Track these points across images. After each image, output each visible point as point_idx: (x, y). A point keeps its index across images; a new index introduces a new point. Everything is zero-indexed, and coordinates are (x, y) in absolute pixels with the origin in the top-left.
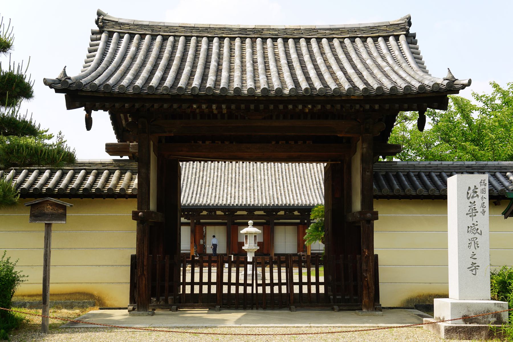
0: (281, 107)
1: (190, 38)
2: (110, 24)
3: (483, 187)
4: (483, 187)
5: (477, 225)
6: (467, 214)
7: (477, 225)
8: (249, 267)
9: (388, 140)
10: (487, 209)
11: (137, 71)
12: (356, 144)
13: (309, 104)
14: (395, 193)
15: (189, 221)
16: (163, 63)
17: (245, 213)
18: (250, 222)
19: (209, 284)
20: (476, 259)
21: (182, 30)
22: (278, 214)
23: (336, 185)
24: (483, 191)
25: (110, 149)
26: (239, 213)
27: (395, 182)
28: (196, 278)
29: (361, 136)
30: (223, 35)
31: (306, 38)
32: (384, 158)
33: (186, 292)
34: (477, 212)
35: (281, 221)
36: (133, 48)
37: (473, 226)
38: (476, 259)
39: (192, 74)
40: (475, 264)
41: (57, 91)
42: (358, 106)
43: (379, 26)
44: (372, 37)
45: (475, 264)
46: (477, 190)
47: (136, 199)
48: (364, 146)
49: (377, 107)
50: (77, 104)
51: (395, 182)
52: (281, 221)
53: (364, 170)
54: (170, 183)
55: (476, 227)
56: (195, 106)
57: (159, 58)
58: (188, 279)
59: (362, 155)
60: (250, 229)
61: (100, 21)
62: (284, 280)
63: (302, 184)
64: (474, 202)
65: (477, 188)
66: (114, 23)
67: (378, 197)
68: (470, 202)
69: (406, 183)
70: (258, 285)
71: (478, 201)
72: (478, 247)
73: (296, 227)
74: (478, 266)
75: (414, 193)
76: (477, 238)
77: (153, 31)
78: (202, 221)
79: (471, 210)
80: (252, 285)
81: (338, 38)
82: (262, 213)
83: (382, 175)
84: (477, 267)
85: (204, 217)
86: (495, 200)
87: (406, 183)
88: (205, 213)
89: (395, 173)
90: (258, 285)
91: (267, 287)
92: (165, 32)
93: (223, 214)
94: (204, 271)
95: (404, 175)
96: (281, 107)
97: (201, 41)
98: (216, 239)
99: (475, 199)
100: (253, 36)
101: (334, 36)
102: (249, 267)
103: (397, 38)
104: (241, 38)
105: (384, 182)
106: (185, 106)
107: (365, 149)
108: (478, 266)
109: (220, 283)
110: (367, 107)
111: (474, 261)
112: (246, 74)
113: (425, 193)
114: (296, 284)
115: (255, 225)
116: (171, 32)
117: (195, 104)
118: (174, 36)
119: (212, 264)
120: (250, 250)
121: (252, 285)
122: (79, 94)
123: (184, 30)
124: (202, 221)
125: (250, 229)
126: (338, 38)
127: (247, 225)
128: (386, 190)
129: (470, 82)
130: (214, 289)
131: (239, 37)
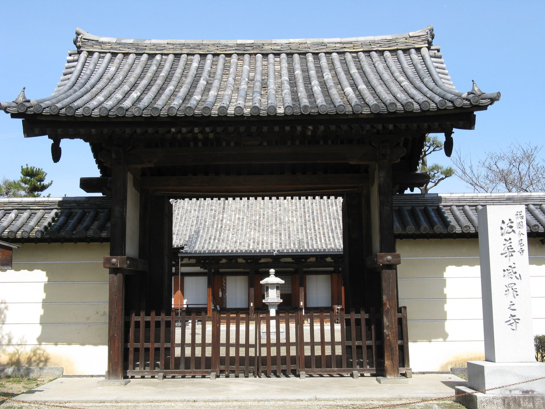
0: (277, 129)
1: (179, 56)
2: (90, 43)
3: (520, 220)
4: (520, 220)
5: (514, 267)
6: (502, 254)
7: (514, 267)
8: (273, 323)
9: (416, 170)
10: (526, 247)
11: (114, 92)
12: (374, 173)
13: (310, 125)
14: (422, 231)
15: (206, 271)
16: (144, 82)
17: (270, 260)
18: (272, 271)
19: (288, 344)
20: (515, 310)
21: (171, 47)
22: (308, 260)
23: (354, 223)
24: (520, 225)
25: (87, 184)
26: (262, 261)
27: (422, 219)
28: (190, 337)
29: (375, 161)
30: (218, 52)
31: (313, 54)
32: (412, 190)
33: (231, 355)
34: (514, 251)
35: (312, 269)
36: (113, 69)
37: (509, 268)
38: (515, 310)
39: (174, 94)
40: (515, 316)
41: (14, 116)
42: (368, 127)
43: (397, 39)
44: (390, 51)
45: (515, 316)
46: (512, 224)
47: (109, 243)
48: (381, 175)
49: (391, 127)
50: (37, 131)
51: (422, 219)
52: (312, 269)
53: (382, 204)
54: (158, 223)
55: (514, 270)
56: (173, 130)
57: (140, 77)
58: (178, 339)
59: (379, 186)
60: (272, 279)
61: (79, 39)
62: (293, 339)
63: (310, 223)
64: (510, 239)
65: (512, 222)
66: (94, 42)
67: (401, 237)
68: (505, 240)
69: (436, 219)
70: (261, 345)
71: (515, 238)
72: (517, 295)
73: (330, 276)
74: (519, 319)
75: (445, 232)
76: (515, 284)
77: (137, 49)
78: (221, 270)
79: (506, 249)
80: (254, 346)
81: (350, 52)
82: (290, 260)
83: (407, 210)
84: (517, 321)
85: (224, 266)
86: (542, 238)
87: (436, 219)
88: (224, 261)
89: (423, 208)
90: (261, 345)
91: (250, 349)
92: (151, 49)
93: (244, 261)
94: (231, 328)
95: (433, 210)
96: (277, 129)
97: (192, 60)
98: (236, 292)
99: (512, 235)
100: (252, 52)
101: (346, 50)
102: (273, 323)
103: (418, 50)
104: (238, 54)
105: (409, 219)
106: (161, 130)
107: (382, 179)
108: (519, 319)
109: (300, 342)
110: (380, 127)
111: (513, 313)
112: (234, 93)
113: (458, 230)
114: (307, 344)
115: (277, 275)
116: (157, 50)
117: (173, 127)
118: (162, 54)
119: (231, 321)
120: (272, 305)
121: (254, 346)
122: (38, 118)
123: (173, 47)
124: (221, 270)
125: (272, 279)
126: (350, 52)
127: (268, 275)
128: (411, 229)
129: (499, 95)
130: (293, 352)
131: (236, 53)
